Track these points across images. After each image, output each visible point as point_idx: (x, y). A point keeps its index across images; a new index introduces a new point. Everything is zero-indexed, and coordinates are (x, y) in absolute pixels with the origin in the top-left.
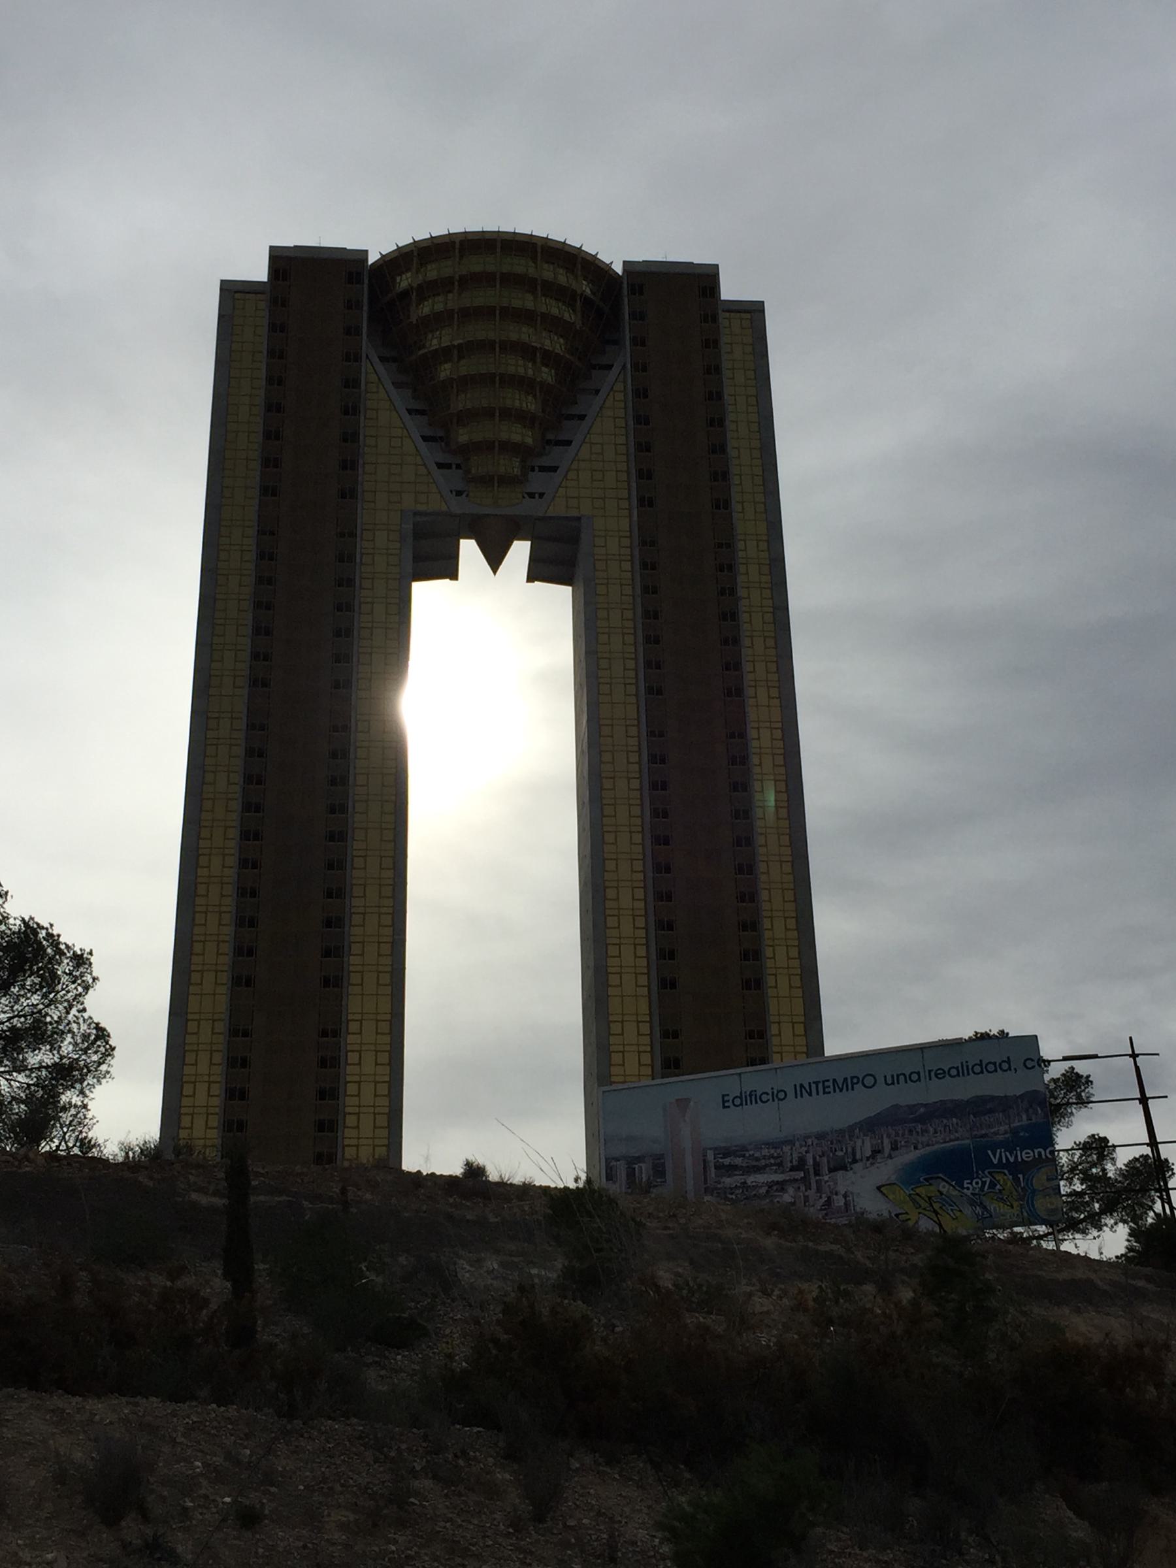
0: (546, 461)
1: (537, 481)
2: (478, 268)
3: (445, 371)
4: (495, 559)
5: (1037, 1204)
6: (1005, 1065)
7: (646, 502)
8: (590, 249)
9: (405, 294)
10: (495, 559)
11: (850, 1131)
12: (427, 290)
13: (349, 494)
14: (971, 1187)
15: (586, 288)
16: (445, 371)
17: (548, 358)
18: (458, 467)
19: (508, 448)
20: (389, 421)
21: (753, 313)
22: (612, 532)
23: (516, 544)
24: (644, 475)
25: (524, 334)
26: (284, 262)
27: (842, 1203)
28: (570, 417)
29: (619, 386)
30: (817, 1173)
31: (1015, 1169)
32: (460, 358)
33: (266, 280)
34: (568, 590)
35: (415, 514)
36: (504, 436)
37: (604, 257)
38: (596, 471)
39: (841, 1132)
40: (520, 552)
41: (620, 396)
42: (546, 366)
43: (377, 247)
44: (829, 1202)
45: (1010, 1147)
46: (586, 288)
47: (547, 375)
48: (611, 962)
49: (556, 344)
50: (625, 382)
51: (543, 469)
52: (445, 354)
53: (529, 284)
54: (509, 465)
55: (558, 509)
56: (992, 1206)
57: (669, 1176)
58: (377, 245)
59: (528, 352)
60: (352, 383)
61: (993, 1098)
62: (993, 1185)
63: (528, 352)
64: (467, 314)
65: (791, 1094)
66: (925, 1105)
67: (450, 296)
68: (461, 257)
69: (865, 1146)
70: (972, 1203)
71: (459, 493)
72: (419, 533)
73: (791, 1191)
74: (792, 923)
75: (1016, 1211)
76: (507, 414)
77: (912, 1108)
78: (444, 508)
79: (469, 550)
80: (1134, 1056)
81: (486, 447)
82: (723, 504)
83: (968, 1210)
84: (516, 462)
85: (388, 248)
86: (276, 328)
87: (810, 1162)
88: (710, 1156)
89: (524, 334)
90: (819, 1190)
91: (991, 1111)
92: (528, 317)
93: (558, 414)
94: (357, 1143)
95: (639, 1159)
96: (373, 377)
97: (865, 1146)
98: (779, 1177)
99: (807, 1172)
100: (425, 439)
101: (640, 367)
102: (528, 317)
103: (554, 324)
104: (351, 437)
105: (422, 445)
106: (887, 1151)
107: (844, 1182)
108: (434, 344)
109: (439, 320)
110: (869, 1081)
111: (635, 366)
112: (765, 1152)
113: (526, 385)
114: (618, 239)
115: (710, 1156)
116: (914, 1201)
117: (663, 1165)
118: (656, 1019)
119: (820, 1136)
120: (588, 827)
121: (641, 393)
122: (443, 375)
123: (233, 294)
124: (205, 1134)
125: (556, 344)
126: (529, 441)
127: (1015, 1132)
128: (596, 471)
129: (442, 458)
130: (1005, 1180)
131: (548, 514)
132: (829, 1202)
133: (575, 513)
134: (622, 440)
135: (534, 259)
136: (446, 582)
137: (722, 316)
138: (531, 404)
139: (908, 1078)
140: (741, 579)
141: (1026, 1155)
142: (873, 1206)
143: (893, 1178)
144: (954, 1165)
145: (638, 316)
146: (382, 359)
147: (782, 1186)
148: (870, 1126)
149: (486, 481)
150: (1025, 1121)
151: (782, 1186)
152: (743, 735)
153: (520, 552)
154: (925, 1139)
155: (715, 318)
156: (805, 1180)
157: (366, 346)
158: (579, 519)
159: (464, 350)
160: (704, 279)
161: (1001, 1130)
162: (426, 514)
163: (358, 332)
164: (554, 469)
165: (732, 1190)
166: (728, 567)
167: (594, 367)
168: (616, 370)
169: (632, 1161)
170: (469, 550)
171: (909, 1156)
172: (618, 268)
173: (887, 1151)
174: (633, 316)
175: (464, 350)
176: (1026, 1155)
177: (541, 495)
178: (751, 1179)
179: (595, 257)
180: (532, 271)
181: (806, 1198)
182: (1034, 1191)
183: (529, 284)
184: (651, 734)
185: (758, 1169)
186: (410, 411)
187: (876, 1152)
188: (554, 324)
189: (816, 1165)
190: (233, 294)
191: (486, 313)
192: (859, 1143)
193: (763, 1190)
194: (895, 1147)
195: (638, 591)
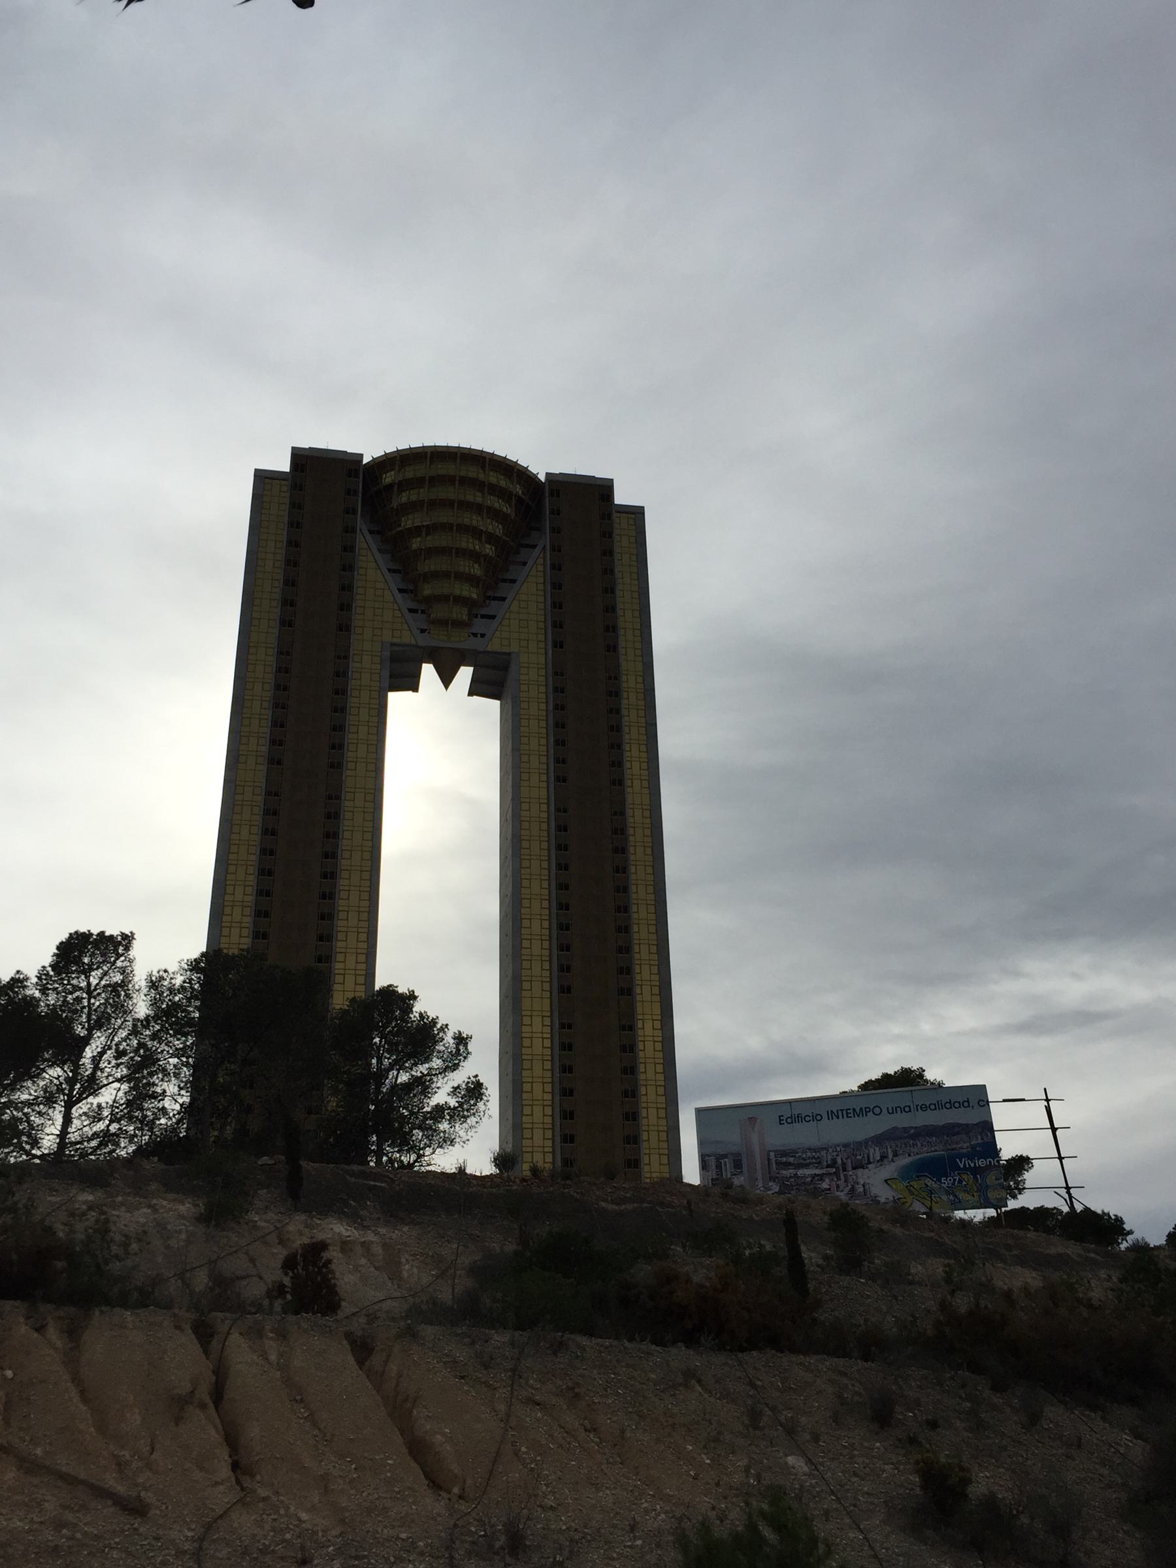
0: (484, 611)
1: (479, 625)
2: (442, 472)
3: (416, 543)
4: (447, 678)
5: (989, 1195)
6: (965, 1104)
7: (558, 644)
8: (523, 463)
9: (390, 487)
10: (447, 678)
11: (866, 1143)
12: (404, 485)
13: (345, 628)
14: (946, 1182)
15: (519, 490)
16: (416, 543)
17: (491, 538)
18: (423, 612)
19: (459, 600)
20: (373, 572)
21: (637, 514)
22: (532, 664)
23: (462, 668)
24: (557, 625)
25: (475, 520)
26: (302, 458)
27: (861, 1190)
28: (505, 581)
29: (541, 561)
30: (845, 1170)
31: (975, 1171)
32: (428, 534)
33: (288, 470)
34: (496, 704)
35: (393, 644)
36: (457, 592)
37: (533, 469)
38: (522, 619)
39: (860, 1143)
40: (465, 674)
41: (541, 568)
42: (490, 543)
43: (370, 453)
44: (853, 1189)
45: (970, 1157)
46: (519, 490)
47: (489, 550)
48: (524, 972)
49: (497, 529)
50: (544, 558)
51: (483, 616)
52: (417, 531)
53: (480, 485)
54: (461, 613)
55: (495, 645)
56: (961, 1195)
57: (745, 1169)
58: (370, 449)
59: (476, 533)
60: (349, 548)
61: (959, 1125)
62: (960, 1181)
63: (476, 533)
64: (433, 504)
65: (825, 1116)
66: (916, 1128)
67: (422, 490)
68: (431, 462)
69: (875, 1153)
70: (948, 1193)
71: (423, 631)
72: (394, 659)
73: (827, 1180)
74: (654, 949)
75: (976, 1198)
76: (460, 577)
77: (905, 1129)
78: (413, 642)
79: (428, 672)
80: (1048, 1100)
81: (444, 599)
82: (613, 648)
83: (945, 1198)
84: (465, 611)
85: (378, 453)
86: (295, 506)
87: (839, 1161)
88: (772, 1154)
89: (475, 520)
90: (846, 1181)
91: (958, 1133)
92: (478, 509)
93: (495, 580)
94: (652, 1168)
95: (725, 1156)
96: (365, 545)
97: (875, 1153)
98: (818, 1172)
99: (837, 1168)
100: (400, 591)
101: (556, 549)
102: (478, 509)
103: (495, 514)
104: (347, 588)
105: (399, 596)
106: (890, 1156)
107: (863, 1176)
108: (409, 524)
109: (414, 506)
110: (877, 1110)
111: (553, 549)
112: (809, 1154)
113: (475, 556)
114: (542, 460)
115: (772, 1154)
116: (910, 1191)
117: (741, 1161)
118: (556, 1014)
119: (845, 1146)
120: (509, 873)
121: (556, 567)
122: (414, 546)
123: (263, 479)
124: (541, 1153)
125: (497, 529)
126: (474, 596)
127: (973, 1147)
128: (522, 619)
129: (413, 605)
130: (968, 1178)
131: (489, 649)
132: (853, 1189)
133: (506, 650)
134: (541, 599)
135: (483, 468)
136: (410, 693)
137: (615, 515)
138: (477, 570)
139: (903, 1110)
140: (624, 702)
141: (981, 1163)
142: (884, 1194)
143: (895, 1175)
144: (935, 1168)
145: (555, 512)
146: (371, 532)
147: (821, 1177)
148: (879, 1140)
149: (443, 623)
150: (980, 1141)
151: (821, 1177)
152: (622, 813)
153: (465, 674)
154: (916, 1150)
155: (609, 516)
156: (836, 1174)
157: (360, 523)
158: (509, 654)
159: (430, 529)
160: (603, 489)
161: (964, 1147)
162: (399, 645)
163: (354, 512)
164: (493, 617)
165: (788, 1179)
166: (615, 694)
167: (522, 546)
168: (538, 550)
169: (719, 1158)
170: (428, 672)
171: (904, 1161)
172: (542, 478)
173: (890, 1156)
174: (552, 512)
175: (430, 529)
176: (981, 1163)
177: (483, 636)
178: (800, 1172)
179: (516, 463)
180: (481, 476)
181: (838, 1186)
182: (987, 1187)
183: (480, 485)
184: (558, 810)
185: (806, 1166)
186: (389, 570)
187: (883, 1157)
188: (495, 514)
189: (843, 1164)
190: (263, 479)
191: (448, 504)
192: (872, 1151)
193: (809, 1179)
194: (896, 1155)
195: (551, 707)
